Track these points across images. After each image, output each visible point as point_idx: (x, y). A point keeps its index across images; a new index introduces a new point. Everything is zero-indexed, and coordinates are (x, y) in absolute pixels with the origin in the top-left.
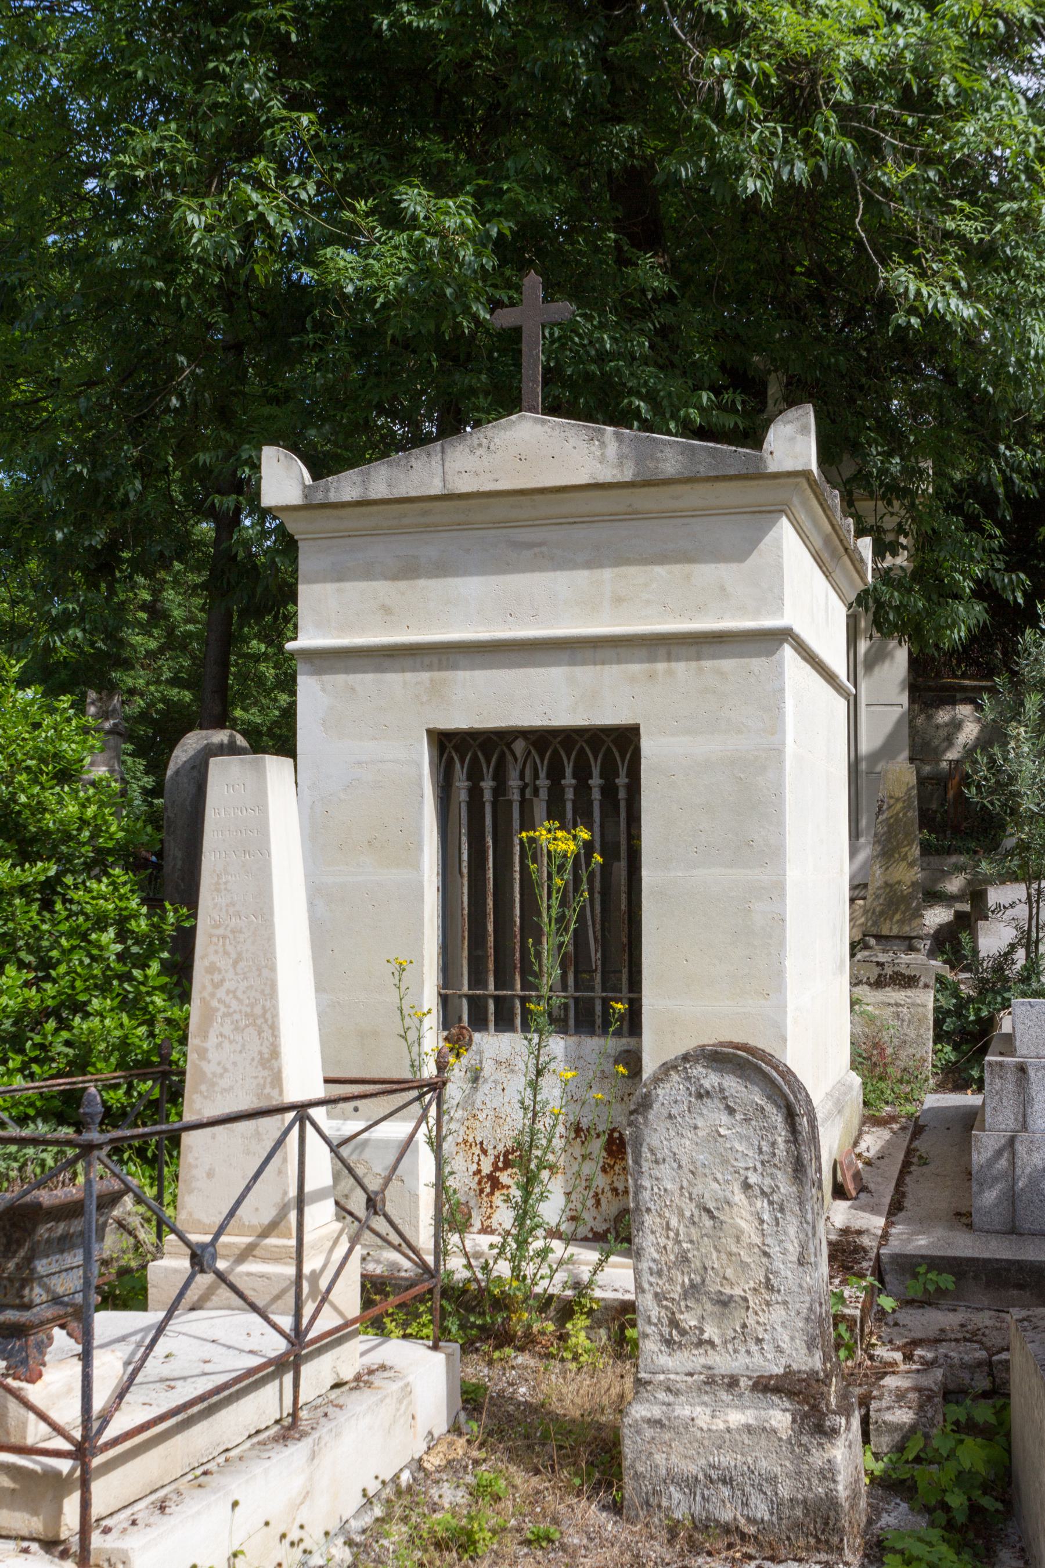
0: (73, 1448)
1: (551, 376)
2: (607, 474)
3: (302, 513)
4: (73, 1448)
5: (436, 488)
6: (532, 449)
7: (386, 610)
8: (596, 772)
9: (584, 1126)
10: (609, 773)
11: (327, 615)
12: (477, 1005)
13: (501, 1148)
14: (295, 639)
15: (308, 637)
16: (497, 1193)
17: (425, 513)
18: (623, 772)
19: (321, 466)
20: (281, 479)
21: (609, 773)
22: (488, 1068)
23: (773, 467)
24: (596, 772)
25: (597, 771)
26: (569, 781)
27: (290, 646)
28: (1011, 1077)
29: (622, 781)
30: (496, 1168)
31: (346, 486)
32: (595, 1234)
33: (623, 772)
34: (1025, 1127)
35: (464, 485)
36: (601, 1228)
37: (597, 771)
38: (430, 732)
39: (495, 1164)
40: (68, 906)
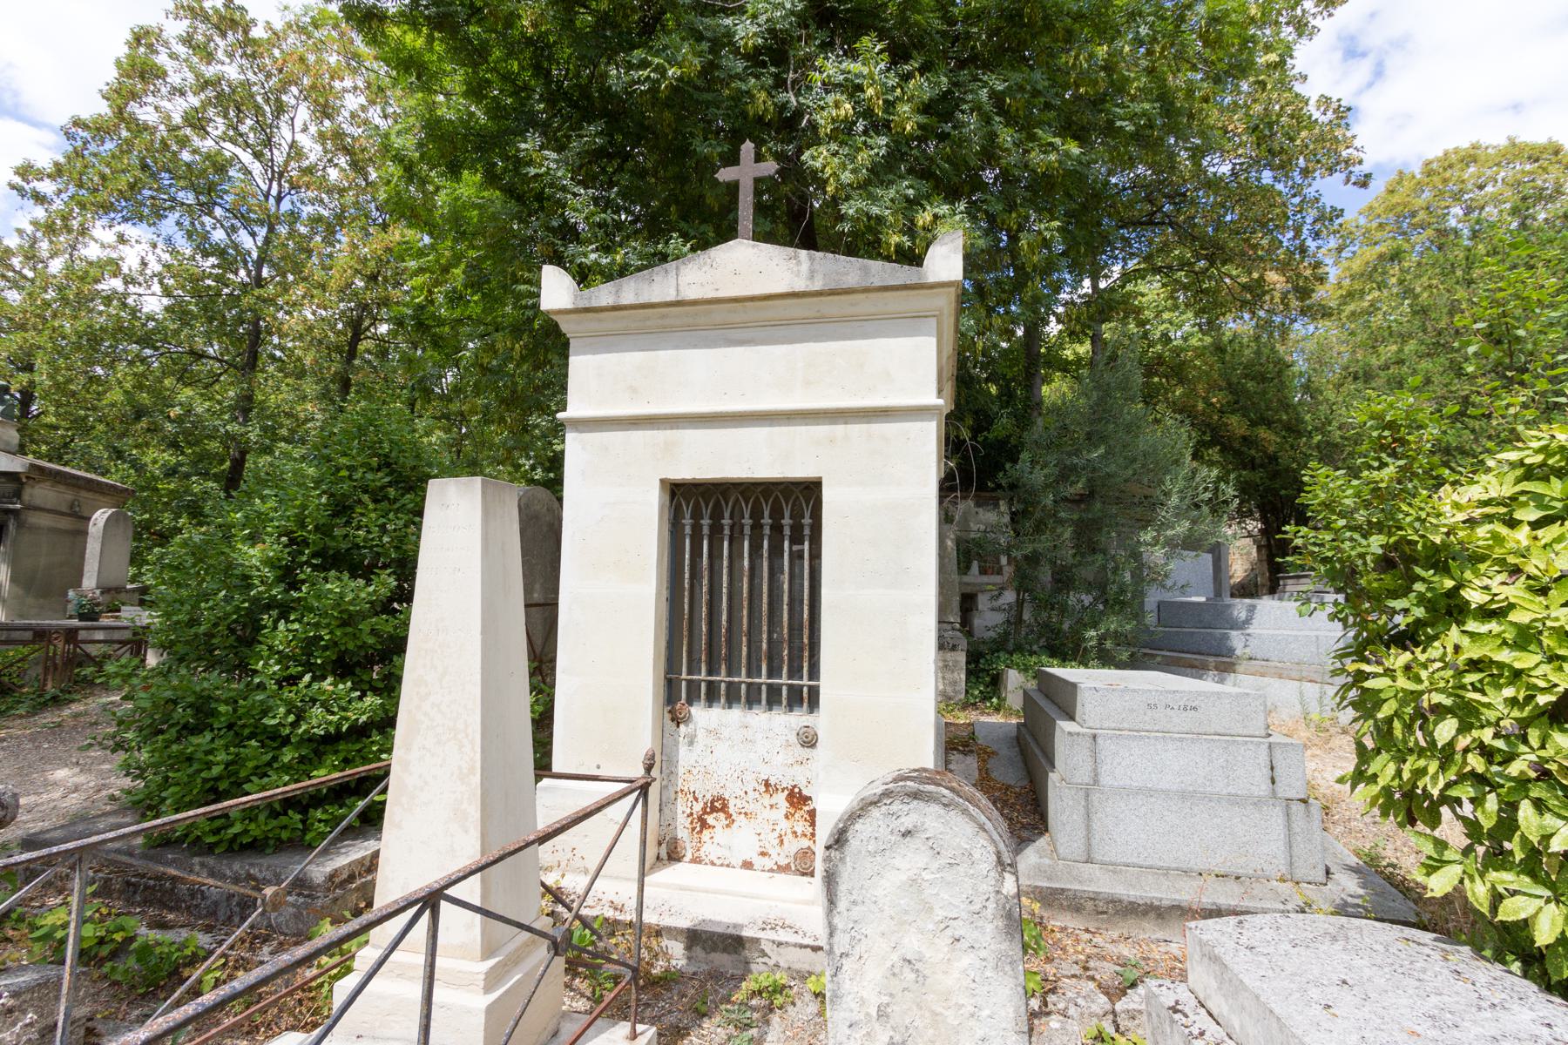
0: (427, 912)
1: (760, 209)
2: (800, 285)
3: (573, 316)
4: (427, 912)
5: (671, 296)
6: (747, 266)
7: (633, 390)
8: (787, 514)
9: (772, 782)
10: (797, 516)
11: (594, 381)
12: (693, 688)
13: (709, 797)
14: (564, 409)
15: (576, 407)
16: (705, 832)
17: (663, 317)
18: (807, 514)
19: (583, 276)
20: (556, 290)
21: (797, 516)
22: (701, 735)
23: (931, 279)
24: (787, 514)
25: (790, 510)
26: (767, 520)
27: (560, 415)
28: (1088, 742)
29: (807, 521)
30: (705, 813)
31: (603, 295)
32: (779, 867)
33: (807, 514)
34: (1096, 782)
35: (691, 294)
36: (783, 862)
37: (790, 510)
38: (663, 481)
39: (704, 809)
40: (275, 765)
